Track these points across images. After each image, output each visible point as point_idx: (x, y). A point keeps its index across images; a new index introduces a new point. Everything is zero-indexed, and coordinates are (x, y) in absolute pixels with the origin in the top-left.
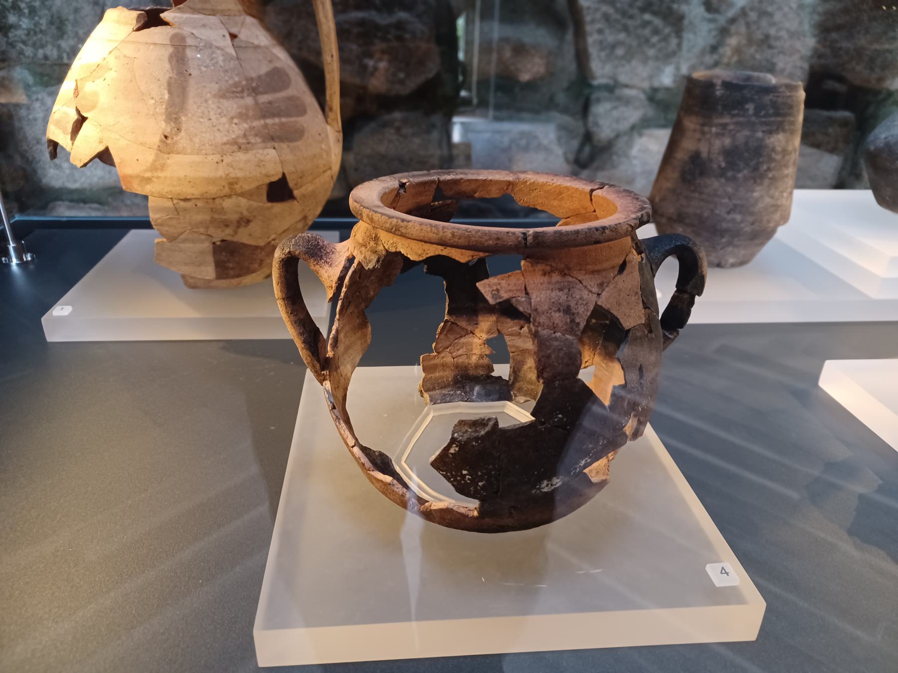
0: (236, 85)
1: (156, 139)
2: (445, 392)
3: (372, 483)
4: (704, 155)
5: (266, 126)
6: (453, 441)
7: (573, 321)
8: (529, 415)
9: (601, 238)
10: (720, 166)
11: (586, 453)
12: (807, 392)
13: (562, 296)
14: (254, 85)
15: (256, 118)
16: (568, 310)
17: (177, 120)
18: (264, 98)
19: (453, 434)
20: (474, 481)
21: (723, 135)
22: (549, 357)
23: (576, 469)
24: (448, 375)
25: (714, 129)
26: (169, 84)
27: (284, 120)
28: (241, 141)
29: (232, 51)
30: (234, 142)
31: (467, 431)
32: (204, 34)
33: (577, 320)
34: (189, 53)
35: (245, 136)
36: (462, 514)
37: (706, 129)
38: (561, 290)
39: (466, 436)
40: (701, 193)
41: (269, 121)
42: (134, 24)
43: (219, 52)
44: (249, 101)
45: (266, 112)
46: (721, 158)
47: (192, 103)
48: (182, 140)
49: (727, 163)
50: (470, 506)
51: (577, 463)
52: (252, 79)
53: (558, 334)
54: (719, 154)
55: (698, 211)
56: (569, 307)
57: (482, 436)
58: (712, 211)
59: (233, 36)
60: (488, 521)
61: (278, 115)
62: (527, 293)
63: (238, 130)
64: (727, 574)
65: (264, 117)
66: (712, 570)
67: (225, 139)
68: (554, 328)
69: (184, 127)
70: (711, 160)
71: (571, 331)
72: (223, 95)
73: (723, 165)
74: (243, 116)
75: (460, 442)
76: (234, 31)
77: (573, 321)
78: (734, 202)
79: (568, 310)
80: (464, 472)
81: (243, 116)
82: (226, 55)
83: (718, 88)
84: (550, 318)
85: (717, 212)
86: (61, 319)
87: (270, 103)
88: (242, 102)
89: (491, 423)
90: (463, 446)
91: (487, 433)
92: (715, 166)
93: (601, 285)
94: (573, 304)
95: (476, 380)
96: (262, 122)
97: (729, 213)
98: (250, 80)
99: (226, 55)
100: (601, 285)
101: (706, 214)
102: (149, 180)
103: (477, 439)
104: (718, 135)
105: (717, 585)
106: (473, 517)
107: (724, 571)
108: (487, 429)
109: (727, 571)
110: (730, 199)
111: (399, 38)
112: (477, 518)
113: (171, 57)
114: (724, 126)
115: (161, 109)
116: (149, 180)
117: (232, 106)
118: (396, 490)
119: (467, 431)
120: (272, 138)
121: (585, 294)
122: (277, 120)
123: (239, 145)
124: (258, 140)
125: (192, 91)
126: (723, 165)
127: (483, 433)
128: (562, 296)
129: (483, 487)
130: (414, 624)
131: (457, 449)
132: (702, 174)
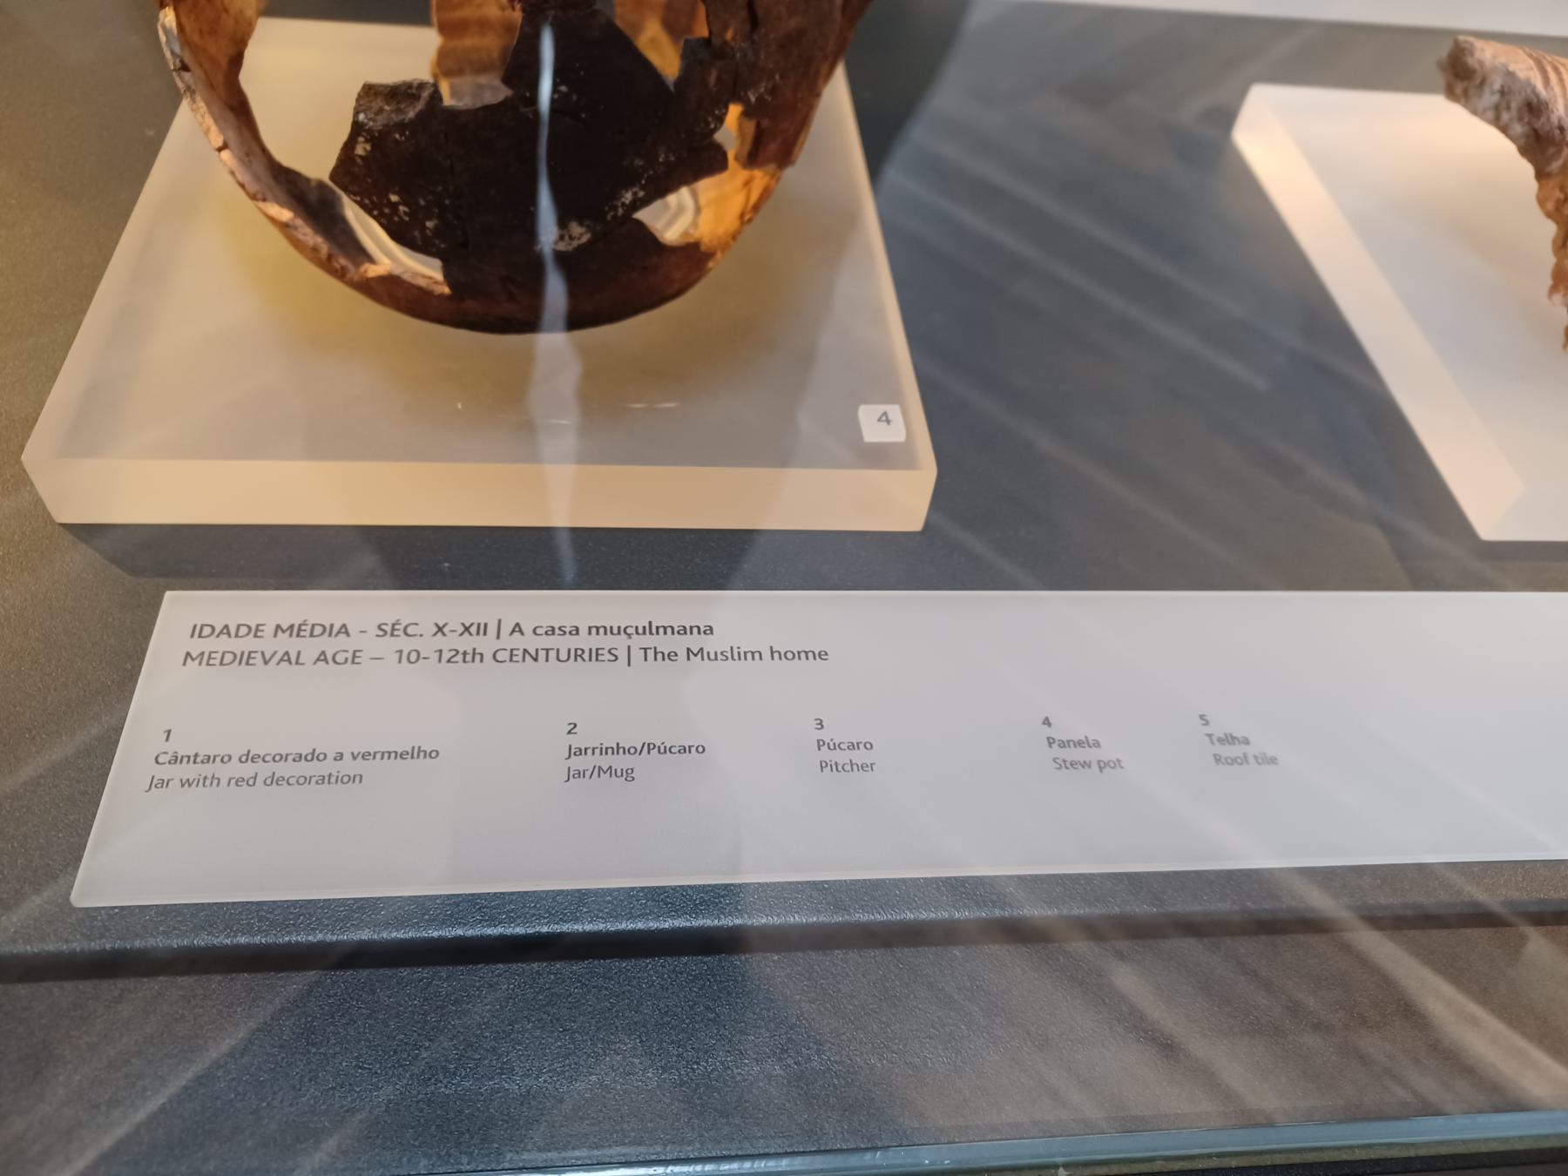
6: (357, 129)
8: (497, 83)
11: (630, 180)
12: (1208, 148)
19: (356, 113)
20: (417, 216)
23: (615, 208)
31: (381, 110)
36: (420, 289)
39: (381, 121)
50: (425, 270)
51: (615, 195)
57: (412, 121)
60: (470, 305)
64: (888, 422)
66: (867, 416)
75: (370, 131)
80: (394, 198)
89: (426, 94)
90: (378, 140)
91: (420, 115)
103: (401, 126)
106: (442, 296)
107: (885, 419)
108: (420, 106)
109: (896, 421)
112: (449, 298)
118: (301, 237)
119: (381, 110)
127: (411, 114)
129: (436, 230)
130: (561, 518)
131: (368, 147)
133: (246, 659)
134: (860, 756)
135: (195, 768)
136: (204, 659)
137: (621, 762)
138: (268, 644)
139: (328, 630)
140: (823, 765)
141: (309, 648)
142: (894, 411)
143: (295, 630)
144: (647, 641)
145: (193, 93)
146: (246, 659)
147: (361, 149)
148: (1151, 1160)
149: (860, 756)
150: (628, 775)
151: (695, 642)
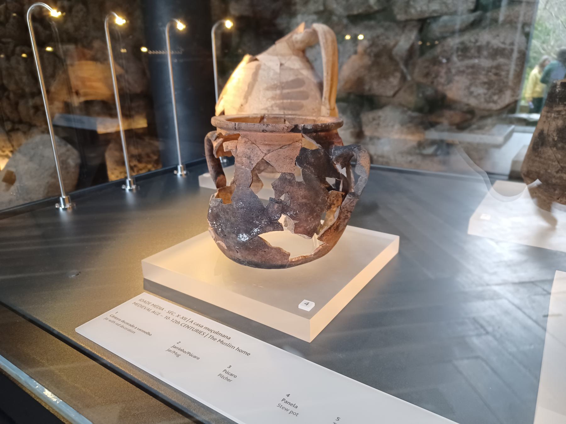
0: (274, 85)
4: (545, 132)
5: (283, 103)
7: (250, 162)
9: (266, 129)
10: (553, 140)
13: (249, 152)
14: (283, 85)
15: (279, 99)
16: (249, 158)
18: (286, 91)
21: (558, 118)
22: (238, 176)
25: (553, 115)
27: (293, 101)
28: (270, 108)
32: (270, 64)
33: (252, 163)
35: (272, 106)
37: (549, 114)
38: (249, 149)
40: (540, 157)
41: (285, 101)
45: (283, 97)
46: (555, 134)
49: (558, 137)
52: (283, 83)
53: (243, 167)
54: (554, 131)
55: (537, 170)
56: (250, 156)
58: (546, 170)
59: (281, 65)
61: (291, 98)
62: (236, 149)
67: (263, 107)
68: (242, 164)
70: (548, 135)
71: (249, 167)
72: (267, 89)
73: (556, 139)
74: (273, 98)
76: (283, 62)
77: (250, 162)
78: (562, 165)
79: (249, 158)
81: (273, 98)
83: (558, 87)
84: (241, 160)
85: (549, 171)
86: (206, 178)
87: (288, 93)
88: (274, 92)
92: (551, 139)
93: (269, 151)
94: (252, 156)
96: (281, 101)
97: (557, 172)
98: (281, 83)
100: (269, 151)
101: (542, 172)
104: (555, 118)
105: (309, 310)
110: (558, 162)
111: (496, 74)
114: (559, 112)
117: (270, 94)
121: (259, 152)
122: (289, 101)
124: (277, 108)
126: (556, 139)
128: (249, 152)
132: (542, 145)
137: (179, 352)
150: (178, 356)
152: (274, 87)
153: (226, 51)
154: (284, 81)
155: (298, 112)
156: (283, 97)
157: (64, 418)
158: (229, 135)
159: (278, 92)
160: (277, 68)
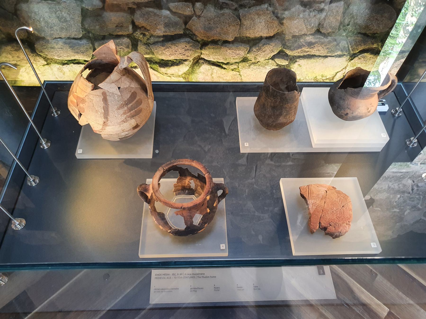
0: (121, 105)
1: (102, 123)
2: (179, 192)
3: (222, 68)
17: (107, 118)
18: (130, 105)
24: (180, 188)
26: (104, 108)
29: (119, 94)
30: (123, 121)
34: (108, 98)
35: (126, 119)
41: (132, 112)
42: (91, 88)
43: (116, 95)
44: (126, 108)
47: (110, 114)
48: (109, 123)
59: (119, 88)
63: (123, 118)
65: (130, 111)
66: (221, 245)
69: (109, 119)
72: (118, 109)
74: (124, 113)
81: (124, 113)
82: (118, 96)
88: (124, 109)
95: (187, 189)
99: (118, 96)
102: (101, 132)
113: (103, 100)
115: (102, 115)
116: (101, 132)
117: (121, 111)
120: (132, 117)
122: (134, 111)
123: (124, 121)
125: (110, 109)
133: (160, 278)
134: (218, 289)
135: (160, 290)
136: (157, 278)
137: (196, 290)
138: (162, 276)
139: (167, 275)
140: (191, 291)
141: (166, 277)
142: (224, 245)
143: (164, 275)
144: (198, 275)
145: (201, 53)
146: (160, 278)
147: (287, 4)
148: (37, 269)
149: (218, 289)
150: (196, 291)
151: (203, 275)
152: (121, 107)
153: (157, 151)
154: (126, 99)
155: (147, 85)
156: (130, 110)
157: (70, 268)
158: (169, 168)
159: (126, 108)
160: (118, 92)
